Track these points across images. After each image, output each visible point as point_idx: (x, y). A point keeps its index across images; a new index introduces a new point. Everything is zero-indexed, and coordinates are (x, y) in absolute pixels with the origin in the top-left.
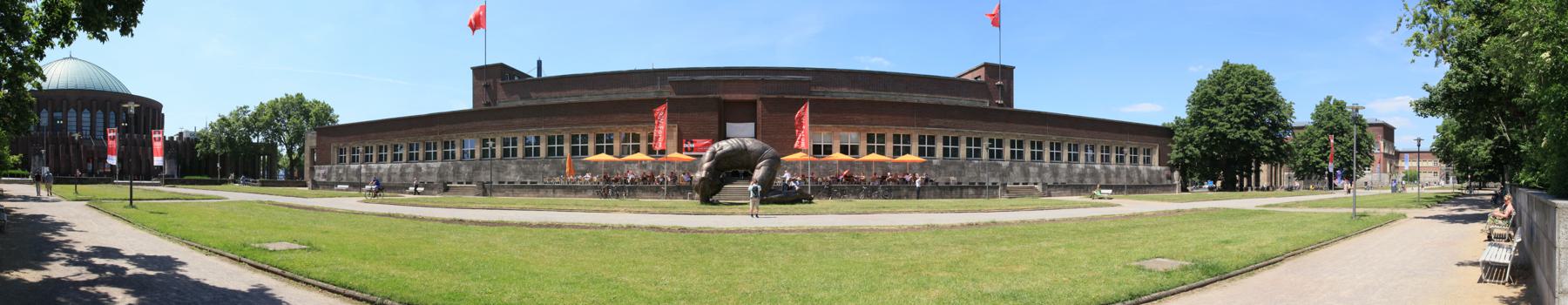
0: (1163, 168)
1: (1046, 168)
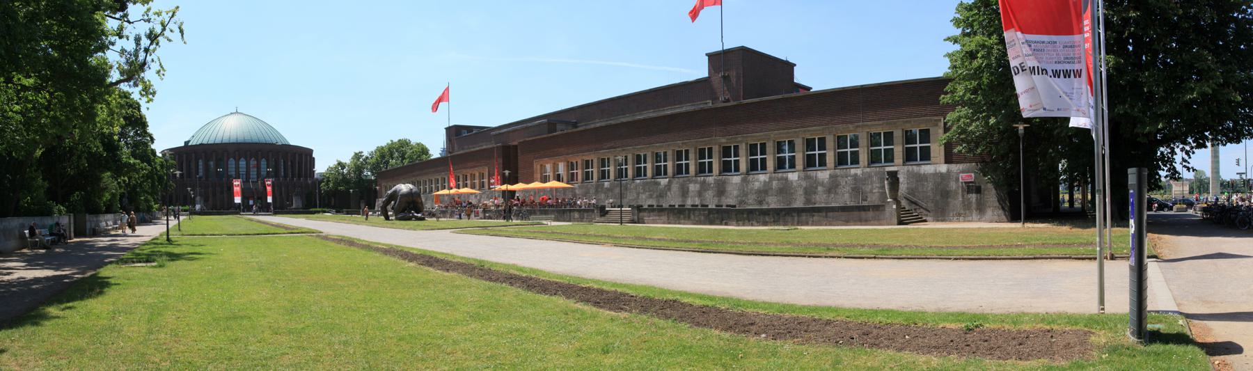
0: (955, 168)
1: (709, 184)
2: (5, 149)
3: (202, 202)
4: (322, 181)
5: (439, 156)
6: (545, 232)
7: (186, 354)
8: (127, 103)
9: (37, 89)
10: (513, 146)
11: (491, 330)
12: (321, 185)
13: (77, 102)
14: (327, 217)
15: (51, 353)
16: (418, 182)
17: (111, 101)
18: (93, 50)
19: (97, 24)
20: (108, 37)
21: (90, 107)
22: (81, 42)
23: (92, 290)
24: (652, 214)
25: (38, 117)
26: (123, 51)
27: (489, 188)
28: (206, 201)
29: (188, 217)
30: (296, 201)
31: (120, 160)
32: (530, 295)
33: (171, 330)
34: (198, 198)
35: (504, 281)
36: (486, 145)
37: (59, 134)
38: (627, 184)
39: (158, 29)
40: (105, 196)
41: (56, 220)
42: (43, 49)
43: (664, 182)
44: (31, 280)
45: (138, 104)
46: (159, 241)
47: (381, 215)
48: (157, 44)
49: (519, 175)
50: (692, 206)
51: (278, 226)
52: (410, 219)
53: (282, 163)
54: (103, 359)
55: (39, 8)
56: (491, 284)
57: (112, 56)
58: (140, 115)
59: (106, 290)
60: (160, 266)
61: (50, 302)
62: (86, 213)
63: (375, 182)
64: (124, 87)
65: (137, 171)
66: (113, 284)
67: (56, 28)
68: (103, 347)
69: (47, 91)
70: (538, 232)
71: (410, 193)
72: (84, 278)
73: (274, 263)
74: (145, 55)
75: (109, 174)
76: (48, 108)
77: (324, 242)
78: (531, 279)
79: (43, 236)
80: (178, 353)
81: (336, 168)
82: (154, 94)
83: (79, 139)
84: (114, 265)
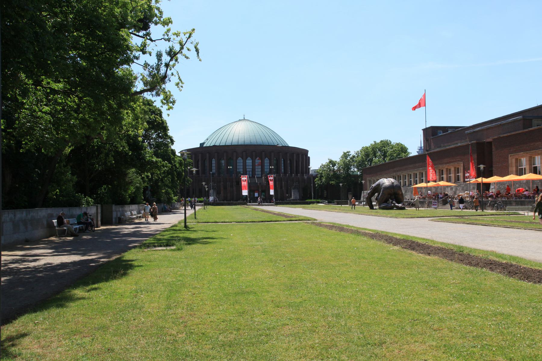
2: (35, 146)
3: (215, 194)
4: (316, 176)
5: (417, 154)
6: (523, 222)
7: (200, 326)
8: (150, 110)
9: (66, 93)
10: (488, 142)
11: (475, 311)
12: (316, 180)
13: (105, 107)
14: (320, 207)
15: (75, 333)
16: (398, 176)
17: (136, 108)
18: (119, 62)
19: (123, 40)
20: (132, 52)
21: (117, 112)
22: (108, 54)
23: (116, 272)
25: (67, 119)
26: (146, 65)
27: (464, 181)
28: (218, 193)
29: (203, 207)
30: (294, 193)
31: (144, 158)
32: (512, 281)
33: (187, 305)
34: (211, 191)
35: (484, 267)
36: (461, 143)
37: (88, 134)
39: (177, 48)
40: (130, 189)
41: (84, 210)
42: (71, 58)
44: (58, 265)
45: (160, 110)
46: (178, 228)
47: (366, 205)
48: (176, 60)
49: (494, 169)
51: (279, 214)
52: (391, 208)
53: (283, 162)
54: (125, 334)
55: (67, 20)
56: (472, 268)
57: (136, 69)
58: (162, 120)
59: (130, 271)
60: (179, 249)
61: (76, 285)
62: (113, 203)
63: (361, 176)
64: (147, 96)
65: (159, 168)
66: (136, 266)
67: (84, 40)
68: (126, 323)
69: (77, 96)
70: (515, 222)
71: (392, 186)
72: (109, 262)
73: (276, 246)
74: (166, 69)
75: (134, 170)
76: (77, 111)
77: (318, 228)
78: (511, 265)
79: (71, 224)
80: (193, 325)
81: (327, 165)
82: (174, 102)
83: (106, 139)
84: (137, 250)
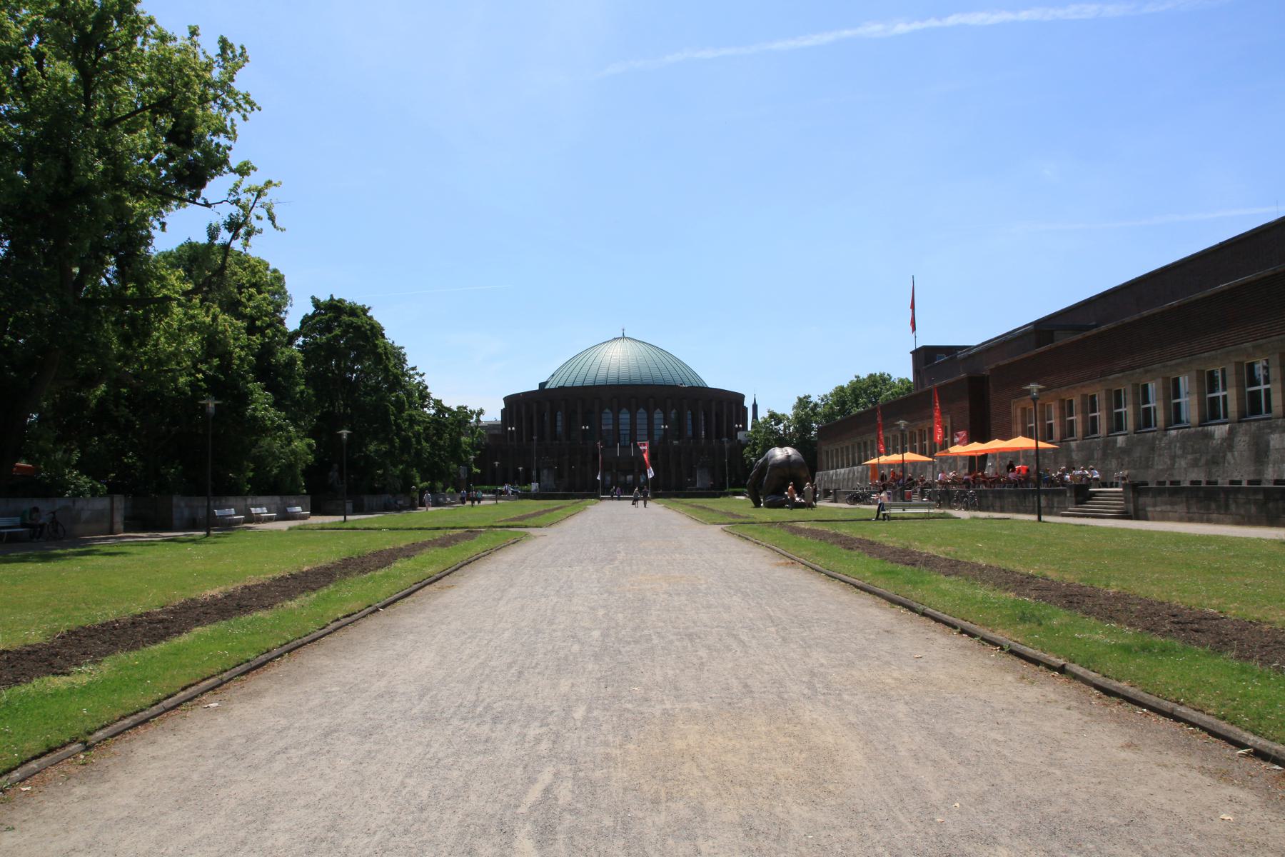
24: (1159, 499)
38: (1154, 438)
43: (1220, 431)
50: (1276, 482)
